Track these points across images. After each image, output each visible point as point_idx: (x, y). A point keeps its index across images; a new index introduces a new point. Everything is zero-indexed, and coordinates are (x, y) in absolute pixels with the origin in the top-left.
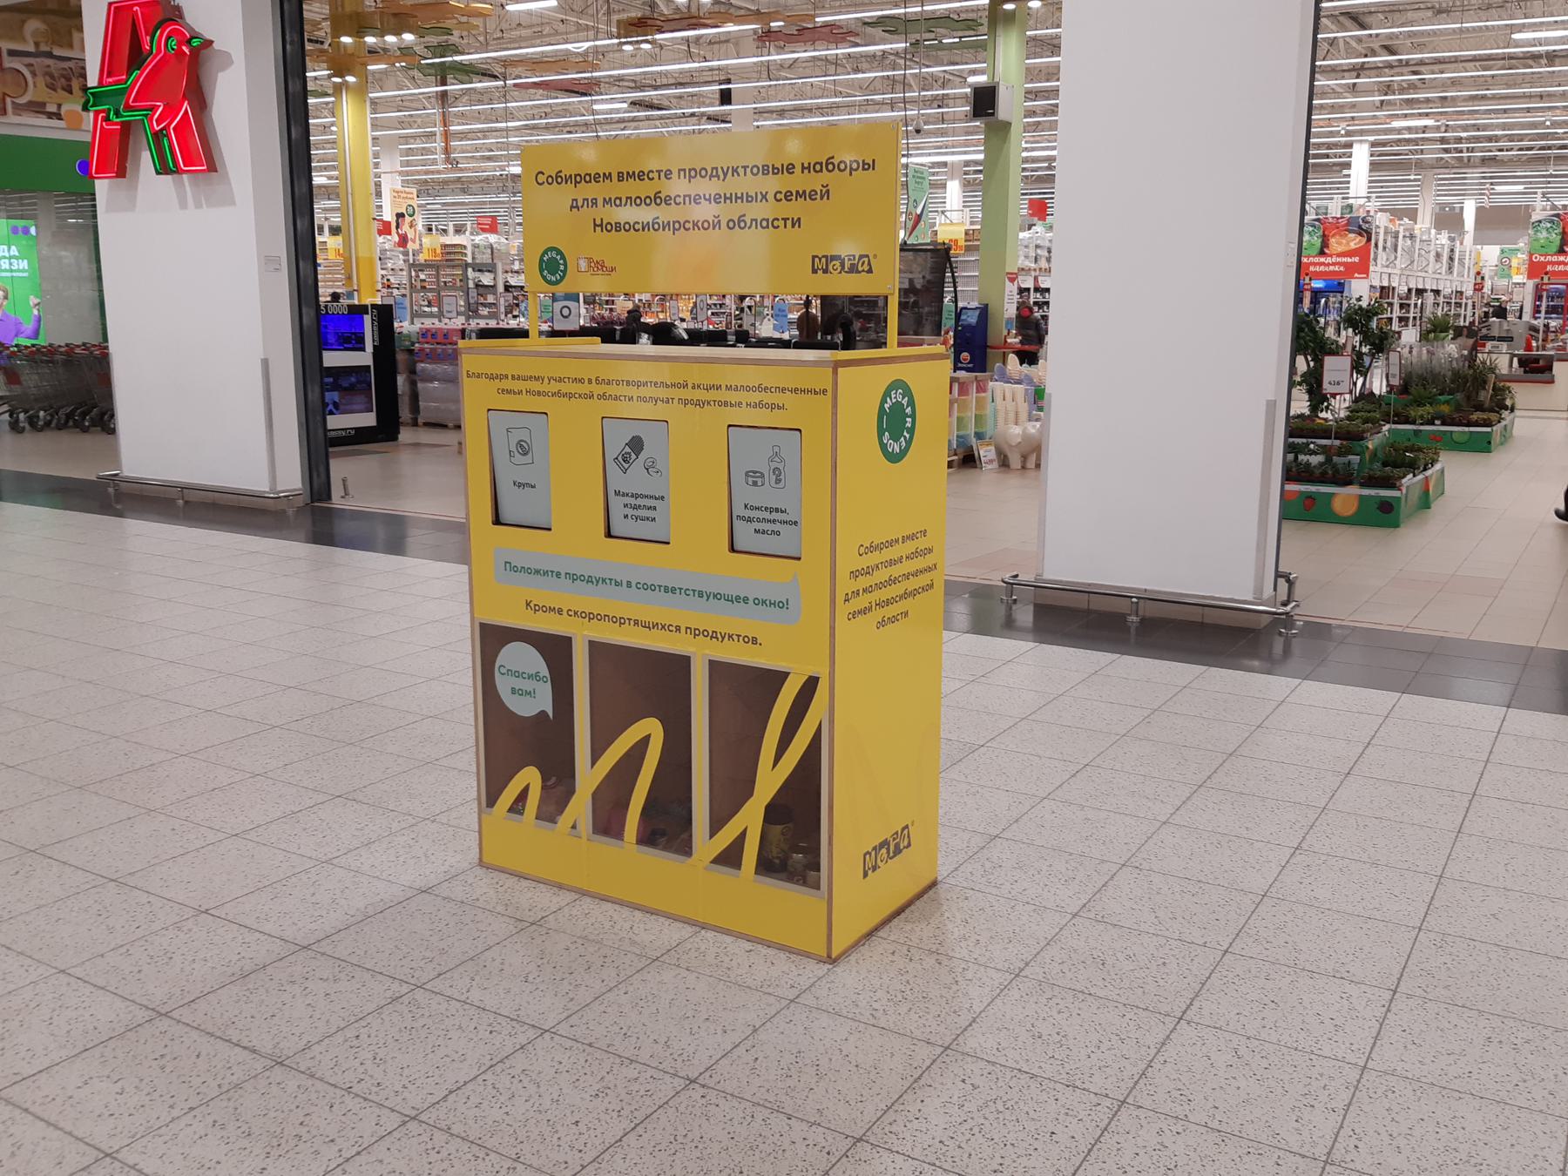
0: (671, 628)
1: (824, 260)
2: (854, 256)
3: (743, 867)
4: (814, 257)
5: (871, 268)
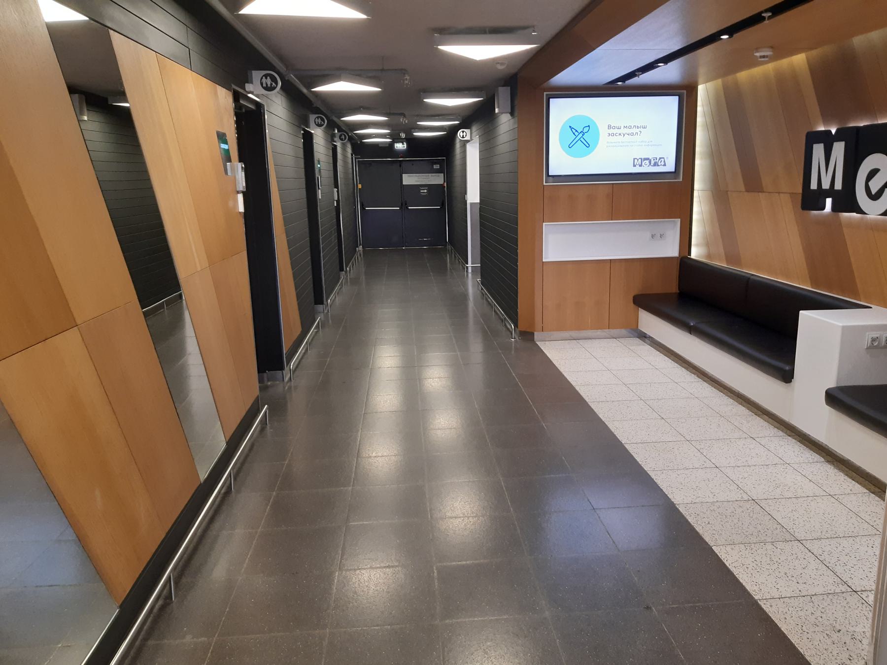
0: (617, 135)
1: (640, 160)
2: (656, 158)
3: (216, 133)
4: (634, 159)
5: (665, 163)
